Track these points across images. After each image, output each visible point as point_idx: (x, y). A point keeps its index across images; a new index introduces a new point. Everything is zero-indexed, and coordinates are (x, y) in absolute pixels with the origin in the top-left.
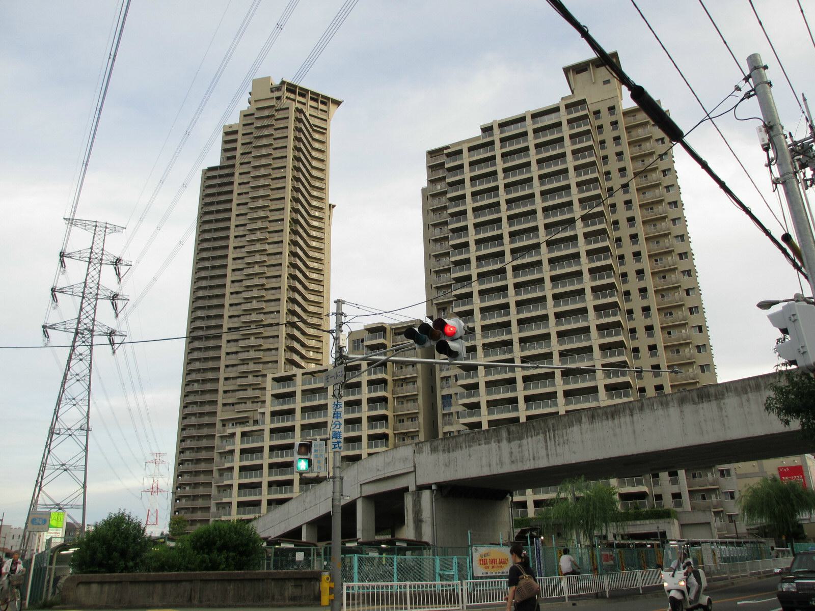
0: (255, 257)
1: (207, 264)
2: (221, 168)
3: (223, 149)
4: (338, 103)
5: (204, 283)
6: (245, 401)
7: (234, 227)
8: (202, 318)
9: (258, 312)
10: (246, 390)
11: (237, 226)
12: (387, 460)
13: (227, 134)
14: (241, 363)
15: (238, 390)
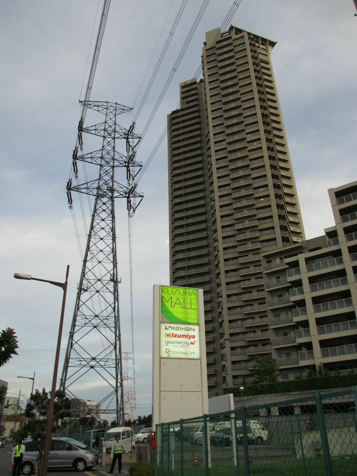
0: (248, 257)
1: (181, 231)
2: (182, 110)
3: (182, 92)
4: (273, 44)
5: (181, 256)
6: (256, 343)
7: (219, 207)
8: (183, 260)
9: (261, 315)
10: (251, 292)
11: (220, 197)
12: (345, 444)
13: (183, 87)
14: (243, 291)
15: (247, 333)
